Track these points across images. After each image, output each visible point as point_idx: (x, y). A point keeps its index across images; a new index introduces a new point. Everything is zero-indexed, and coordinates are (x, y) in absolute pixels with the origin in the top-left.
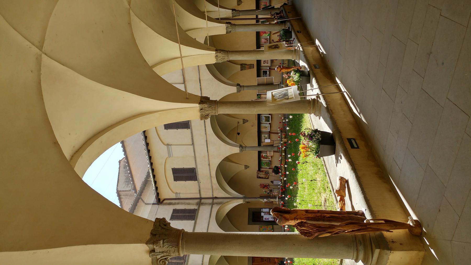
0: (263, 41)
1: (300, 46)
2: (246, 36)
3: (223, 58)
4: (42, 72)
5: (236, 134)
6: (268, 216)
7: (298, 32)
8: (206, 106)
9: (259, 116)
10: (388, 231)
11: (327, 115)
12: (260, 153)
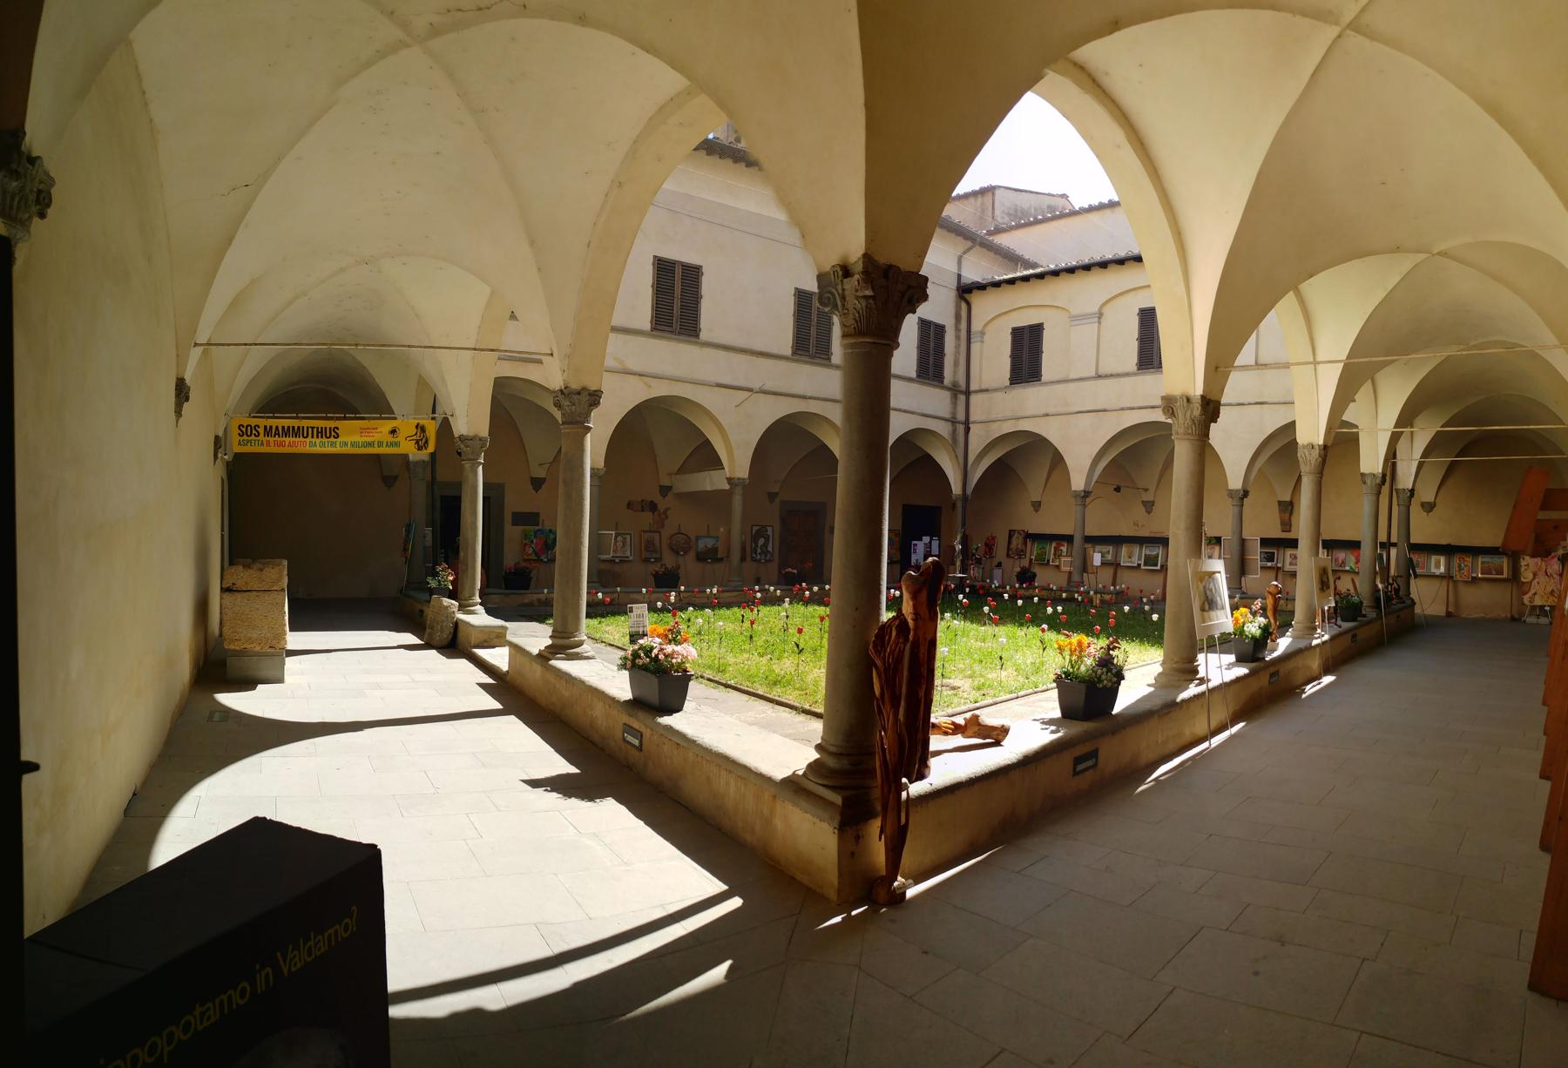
0: (1341, 555)
2: (1354, 517)
3: (1308, 462)
4: (1298, 18)
6: (924, 552)
7: (1354, 636)
9: (1164, 542)
11: (1158, 702)
12: (1069, 539)
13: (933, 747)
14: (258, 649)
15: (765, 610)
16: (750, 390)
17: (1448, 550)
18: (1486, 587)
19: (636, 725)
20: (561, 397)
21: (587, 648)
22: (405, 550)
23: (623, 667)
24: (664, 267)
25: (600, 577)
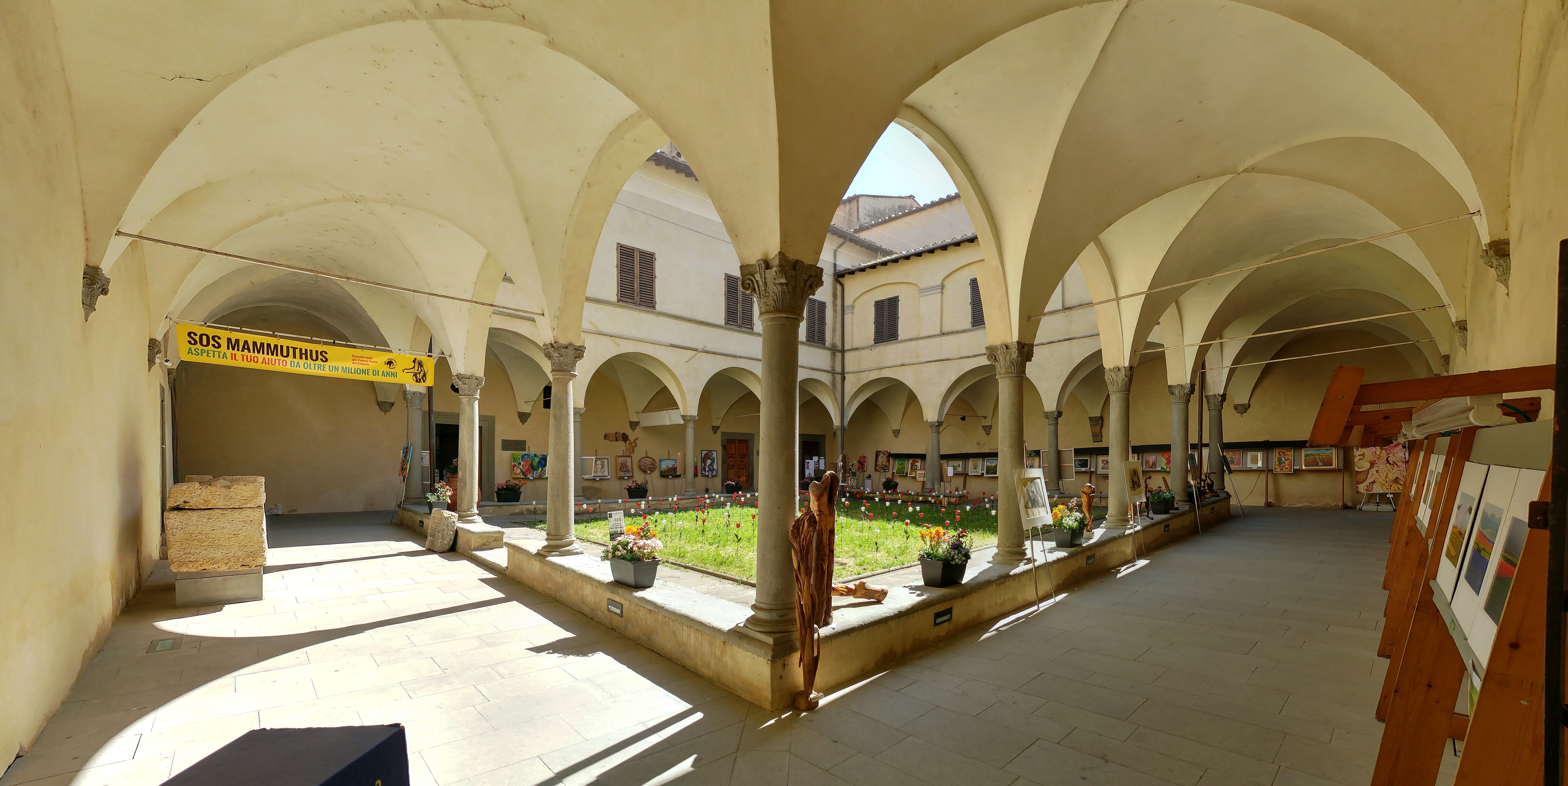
0: (1151, 458)
1: (1136, 529)
2: (1163, 424)
3: (1114, 383)
5: (962, 414)
7: (1167, 526)
8: (1014, 353)
10: (801, 660)
11: (994, 575)
12: (923, 457)
13: (833, 604)
14: (224, 568)
15: (712, 512)
16: (696, 350)
17: (1266, 446)
18: (1311, 479)
19: (617, 599)
20: (551, 350)
21: (577, 546)
22: (403, 469)
23: (605, 558)
24: (626, 254)
25: (586, 492)
